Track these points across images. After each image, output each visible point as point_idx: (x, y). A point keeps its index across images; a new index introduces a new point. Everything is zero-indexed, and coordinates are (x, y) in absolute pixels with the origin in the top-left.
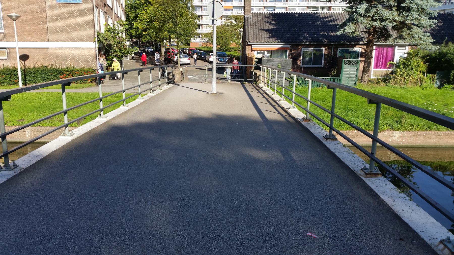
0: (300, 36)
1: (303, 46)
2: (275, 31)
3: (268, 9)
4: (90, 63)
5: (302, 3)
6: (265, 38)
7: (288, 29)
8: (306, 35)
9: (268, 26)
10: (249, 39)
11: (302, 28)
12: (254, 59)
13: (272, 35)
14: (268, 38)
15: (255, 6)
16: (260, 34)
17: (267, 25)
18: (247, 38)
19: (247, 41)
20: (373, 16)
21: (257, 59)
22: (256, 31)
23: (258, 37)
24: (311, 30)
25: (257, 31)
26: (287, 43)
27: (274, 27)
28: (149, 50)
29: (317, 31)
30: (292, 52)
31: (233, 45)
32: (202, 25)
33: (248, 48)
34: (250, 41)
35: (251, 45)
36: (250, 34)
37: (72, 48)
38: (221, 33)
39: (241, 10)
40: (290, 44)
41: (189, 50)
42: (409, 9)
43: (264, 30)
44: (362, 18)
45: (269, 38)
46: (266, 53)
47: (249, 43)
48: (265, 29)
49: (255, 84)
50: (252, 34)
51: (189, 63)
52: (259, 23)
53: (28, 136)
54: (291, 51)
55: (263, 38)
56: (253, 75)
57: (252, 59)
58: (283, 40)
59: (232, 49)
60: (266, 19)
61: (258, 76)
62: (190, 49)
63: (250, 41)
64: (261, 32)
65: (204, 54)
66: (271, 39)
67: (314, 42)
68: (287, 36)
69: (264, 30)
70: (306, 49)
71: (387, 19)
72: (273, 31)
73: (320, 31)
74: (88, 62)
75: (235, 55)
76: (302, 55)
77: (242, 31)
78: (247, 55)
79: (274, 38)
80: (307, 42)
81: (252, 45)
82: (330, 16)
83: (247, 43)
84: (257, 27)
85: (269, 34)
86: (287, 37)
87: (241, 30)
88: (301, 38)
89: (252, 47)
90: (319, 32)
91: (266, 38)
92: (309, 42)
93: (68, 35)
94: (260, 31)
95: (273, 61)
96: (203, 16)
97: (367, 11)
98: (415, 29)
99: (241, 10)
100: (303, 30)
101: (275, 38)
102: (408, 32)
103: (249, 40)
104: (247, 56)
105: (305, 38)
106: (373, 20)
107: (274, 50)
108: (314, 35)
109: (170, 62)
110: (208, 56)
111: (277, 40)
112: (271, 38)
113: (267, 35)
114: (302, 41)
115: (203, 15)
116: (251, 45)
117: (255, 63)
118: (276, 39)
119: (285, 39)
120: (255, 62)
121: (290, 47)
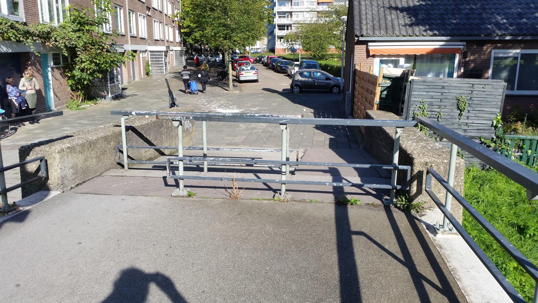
0: (487, 22)
1: (494, 45)
2: (424, 12)
6: (401, 27)
7: (453, 7)
10: (361, 29)
11: (488, 4)
12: (380, 80)
13: (417, 20)
14: (408, 27)
16: (389, 18)
18: (357, 27)
19: (357, 33)
21: (389, 78)
22: (378, 11)
23: (384, 25)
24: (510, 9)
25: (380, 12)
26: (455, 38)
27: (421, 2)
28: (217, 59)
29: (527, 11)
30: (468, 59)
31: (332, 49)
32: (291, 26)
33: (359, 51)
34: (364, 33)
35: (365, 43)
36: (364, 17)
40: (461, 41)
41: (268, 58)
43: (396, 8)
45: (411, 25)
46: (402, 61)
47: (361, 39)
48: (400, 6)
49: (406, 210)
50: (370, 17)
51: (256, 79)
54: (464, 55)
55: (397, 28)
56: (396, 168)
57: (372, 80)
58: (445, 29)
59: (331, 57)
61: (420, 173)
62: (270, 57)
63: (365, 34)
64: (391, 14)
65: (286, 63)
66: (417, 29)
67: (525, 35)
68: (454, 21)
69: (396, 8)
70: (501, 53)
72: (419, 12)
73: (534, 11)
75: (333, 65)
76: (492, 66)
77: (346, 20)
78: (357, 67)
79: (423, 25)
80: (505, 35)
81: (370, 44)
83: (356, 39)
85: (410, 18)
86: (453, 23)
87: (344, 19)
88: (489, 26)
89: (370, 48)
90: (533, 13)
91: (403, 26)
92: (511, 35)
94: (388, 12)
95: (443, 87)
96: (293, 13)
100: (490, 9)
101: (425, 27)
103: (361, 32)
104: (356, 70)
107: (415, 55)
108: (522, 18)
109: (225, 78)
110: (290, 67)
111: (431, 30)
112: (414, 27)
113: (404, 19)
114: (494, 32)
115: (292, 12)
116: (365, 43)
117: (382, 92)
118: (427, 27)
119: (450, 28)
120: (383, 89)
121: (462, 47)
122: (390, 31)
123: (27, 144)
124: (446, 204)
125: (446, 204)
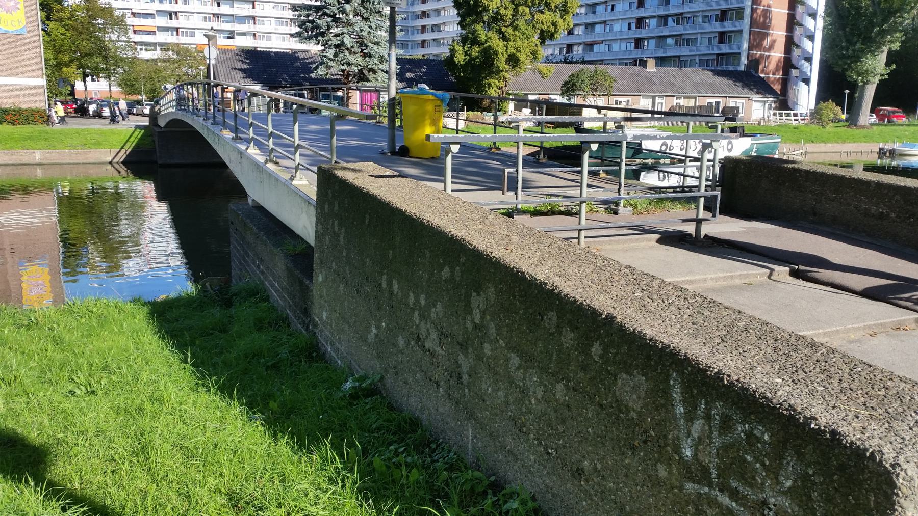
3: (222, 35)
4: (38, 103)
5: (281, 27)
8: (285, 76)
9: (239, 65)
15: (198, 29)
17: (239, 64)
20: (341, 60)
36: (219, 72)
37: (16, 85)
38: (155, 72)
39: (172, 35)
42: (370, 56)
43: (235, 69)
44: (332, 62)
45: (244, 78)
50: (223, 74)
52: (229, 60)
53: (37, 158)
58: (258, 80)
60: (237, 57)
69: (235, 69)
71: (353, 64)
74: (36, 101)
79: (249, 78)
82: (312, 57)
84: (227, 65)
93: (10, 69)
94: (231, 71)
97: (336, 55)
98: (380, 73)
99: (172, 35)
102: (374, 75)
105: (284, 79)
106: (341, 64)
113: (241, 75)
122: (233, 80)
123: (565, 132)
124: (817, 8)
125: (817, 8)
